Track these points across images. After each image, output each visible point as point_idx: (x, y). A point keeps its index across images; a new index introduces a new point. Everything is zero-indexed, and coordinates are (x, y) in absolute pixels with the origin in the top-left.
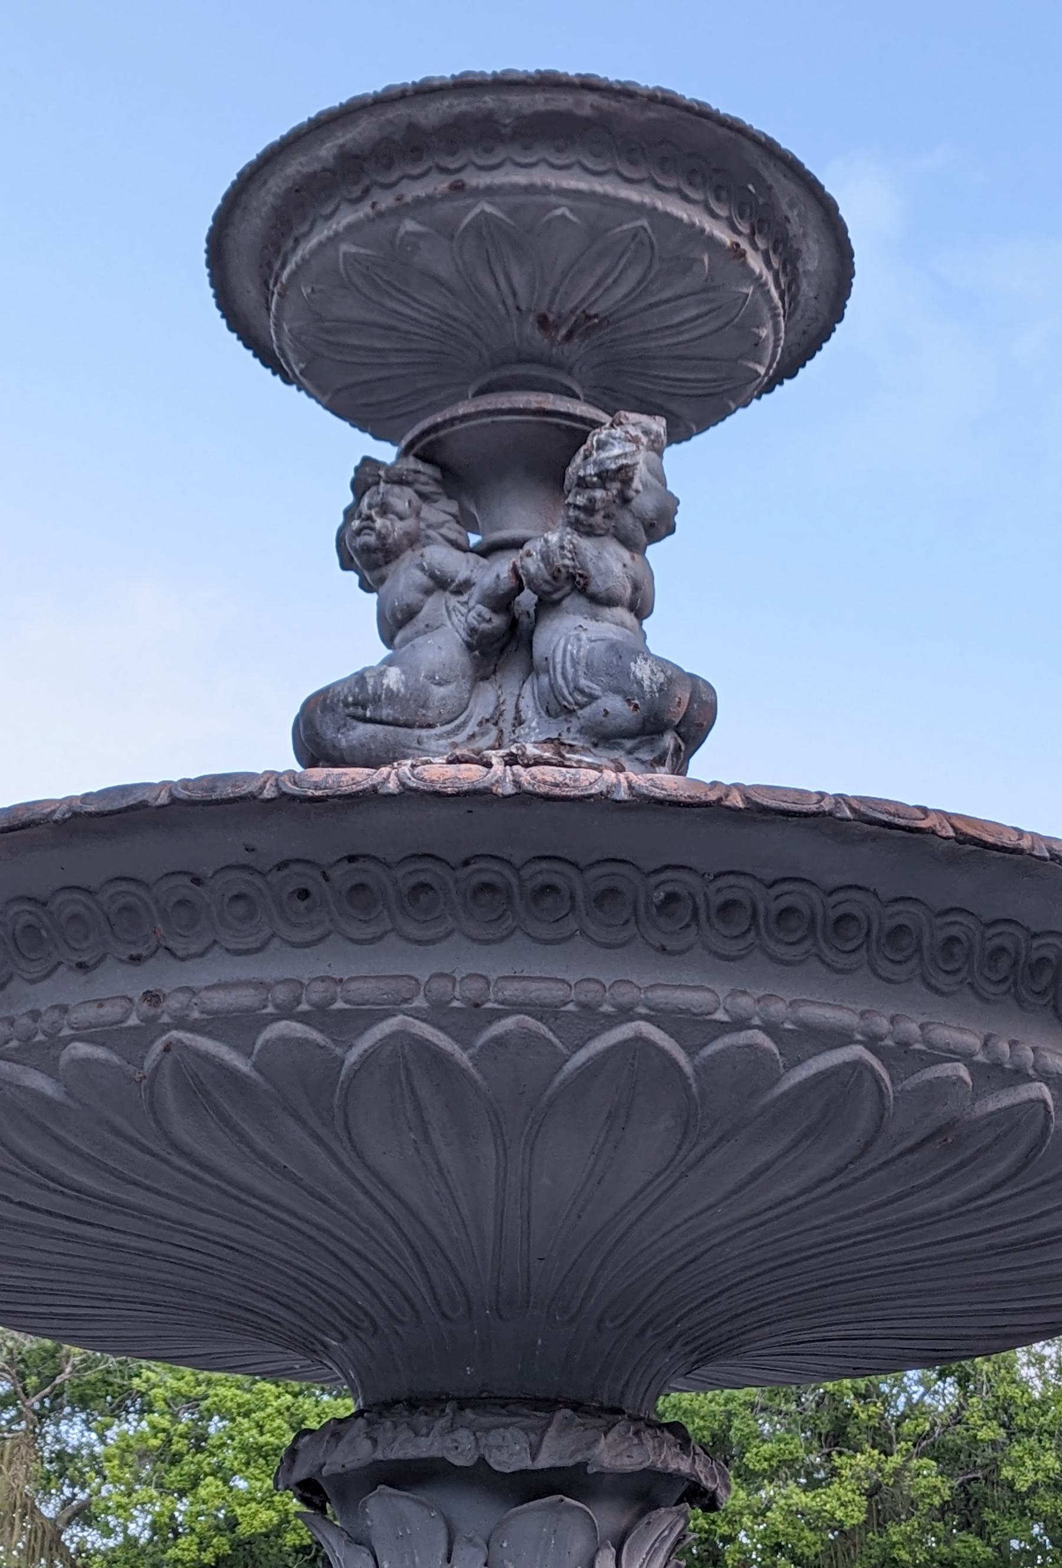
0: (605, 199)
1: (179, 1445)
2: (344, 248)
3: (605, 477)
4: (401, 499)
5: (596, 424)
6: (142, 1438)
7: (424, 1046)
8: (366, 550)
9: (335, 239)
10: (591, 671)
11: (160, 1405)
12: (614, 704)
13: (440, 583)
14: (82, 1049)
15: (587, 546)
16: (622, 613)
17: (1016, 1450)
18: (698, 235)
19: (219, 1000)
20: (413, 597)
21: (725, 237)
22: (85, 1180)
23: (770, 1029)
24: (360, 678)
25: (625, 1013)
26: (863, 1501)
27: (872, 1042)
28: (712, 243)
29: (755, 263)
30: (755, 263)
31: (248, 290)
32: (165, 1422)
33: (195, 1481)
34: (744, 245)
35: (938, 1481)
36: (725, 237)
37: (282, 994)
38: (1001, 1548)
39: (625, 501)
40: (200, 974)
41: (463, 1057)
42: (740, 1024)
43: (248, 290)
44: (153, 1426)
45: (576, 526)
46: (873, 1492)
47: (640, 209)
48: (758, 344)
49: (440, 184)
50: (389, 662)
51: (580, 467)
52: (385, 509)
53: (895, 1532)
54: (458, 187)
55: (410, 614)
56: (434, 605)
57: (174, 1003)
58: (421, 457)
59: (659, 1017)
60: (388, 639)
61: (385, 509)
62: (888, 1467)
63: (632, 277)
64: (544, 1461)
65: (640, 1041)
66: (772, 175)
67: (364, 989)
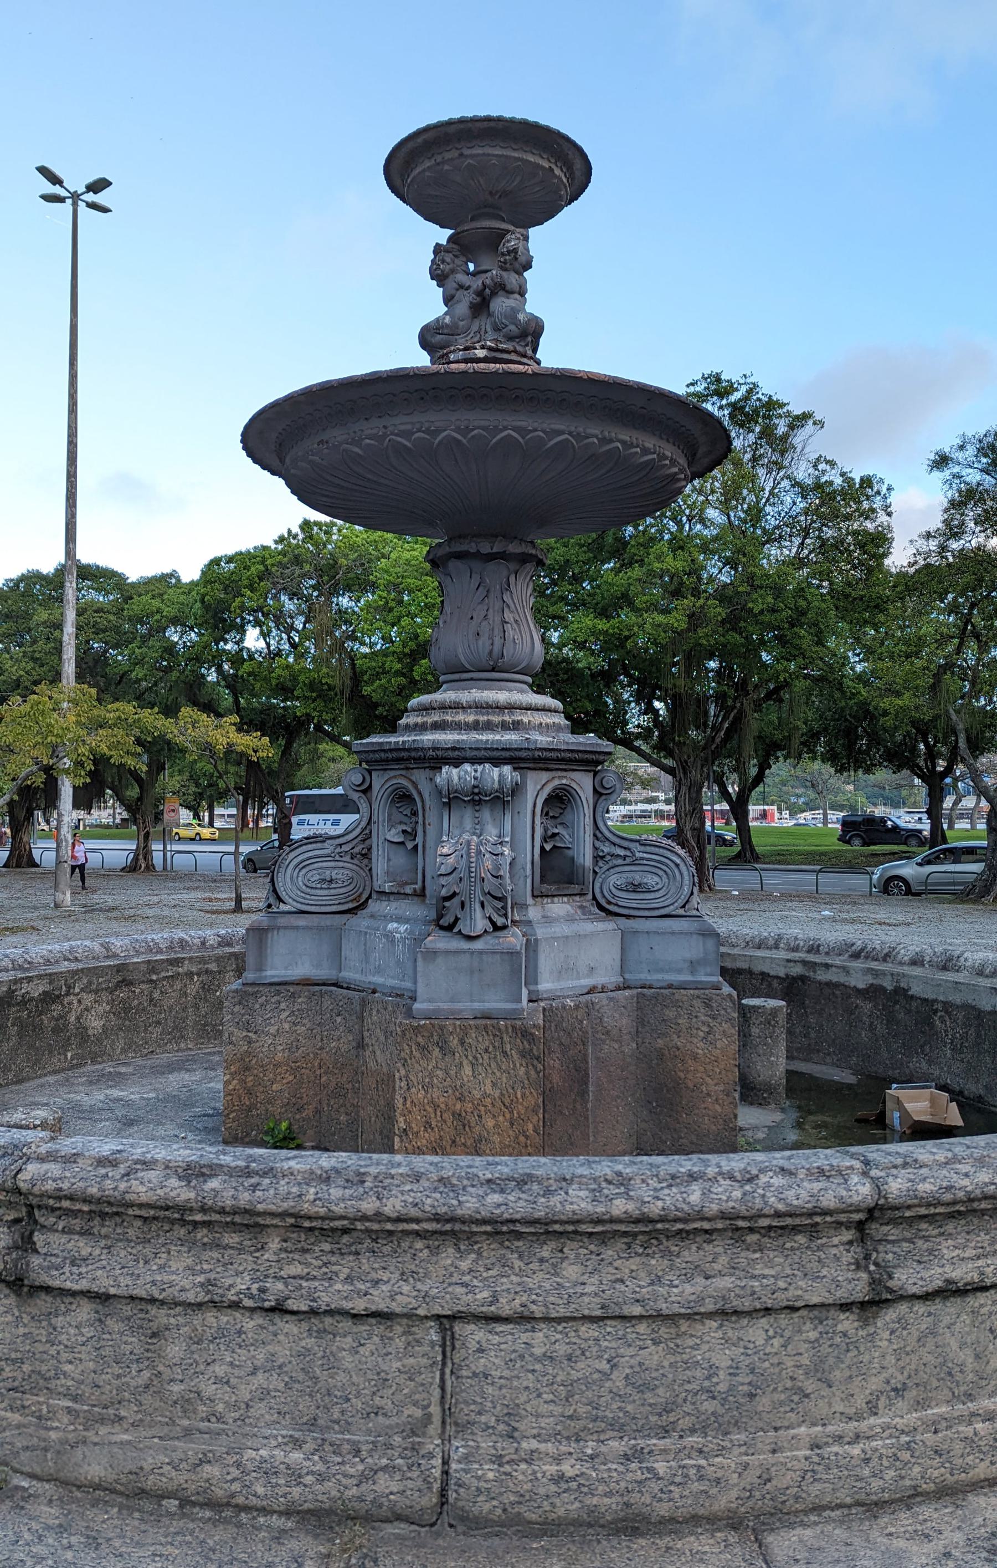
0: (507, 157)
1: (391, 604)
2: (427, 174)
3: (509, 252)
4: (448, 258)
5: (508, 231)
6: (375, 601)
7: (455, 438)
8: (438, 275)
9: (424, 171)
10: (506, 317)
11: (382, 587)
12: (512, 327)
13: (461, 287)
14: (368, 441)
15: (504, 274)
16: (517, 296)
17: (755, 596)
18: (538, 166)
19: (402, 427)
20: (453, 292)
21: (546, 164)
22: (369, 476)
23: (544, 431)
24: (437, 320)
25: (505, 428)
26: (686, 619)
27: (570, 433)
28: (542, 168)
29: (557, 172)
30: (557, 172)
31: (398, 182)
32: (385, 594)
33: (399, 619)
34: (553, 166)
35: (719, 610)
36: (546, 164)
37: (418, 426)
38: (748, 638)
39: (516, 259)
40: (397, 421)
41: (464, 441)
42: (536, 430)
43: (398, 182)
44: (380, 596)
45: (501, 267)
46: (691, 616)
47: (518, 159)
48: (561, 196)
49: (455, 154)
50: (446, 314)
51: (503, 249)
52: (443, 261)
53: (701, 632)
54: (461, 155)
55: (453, 297)
56: (459, 294)
57: (391, 428)
58: (454, 243)
59: (514, 429)
60: (446, 304)
61: (443, 261)
62: (698, 605)
63: (518, 179)
64: (495, 550)
65: (509, 435)
66: (561, 141)
67: (437, 424)
